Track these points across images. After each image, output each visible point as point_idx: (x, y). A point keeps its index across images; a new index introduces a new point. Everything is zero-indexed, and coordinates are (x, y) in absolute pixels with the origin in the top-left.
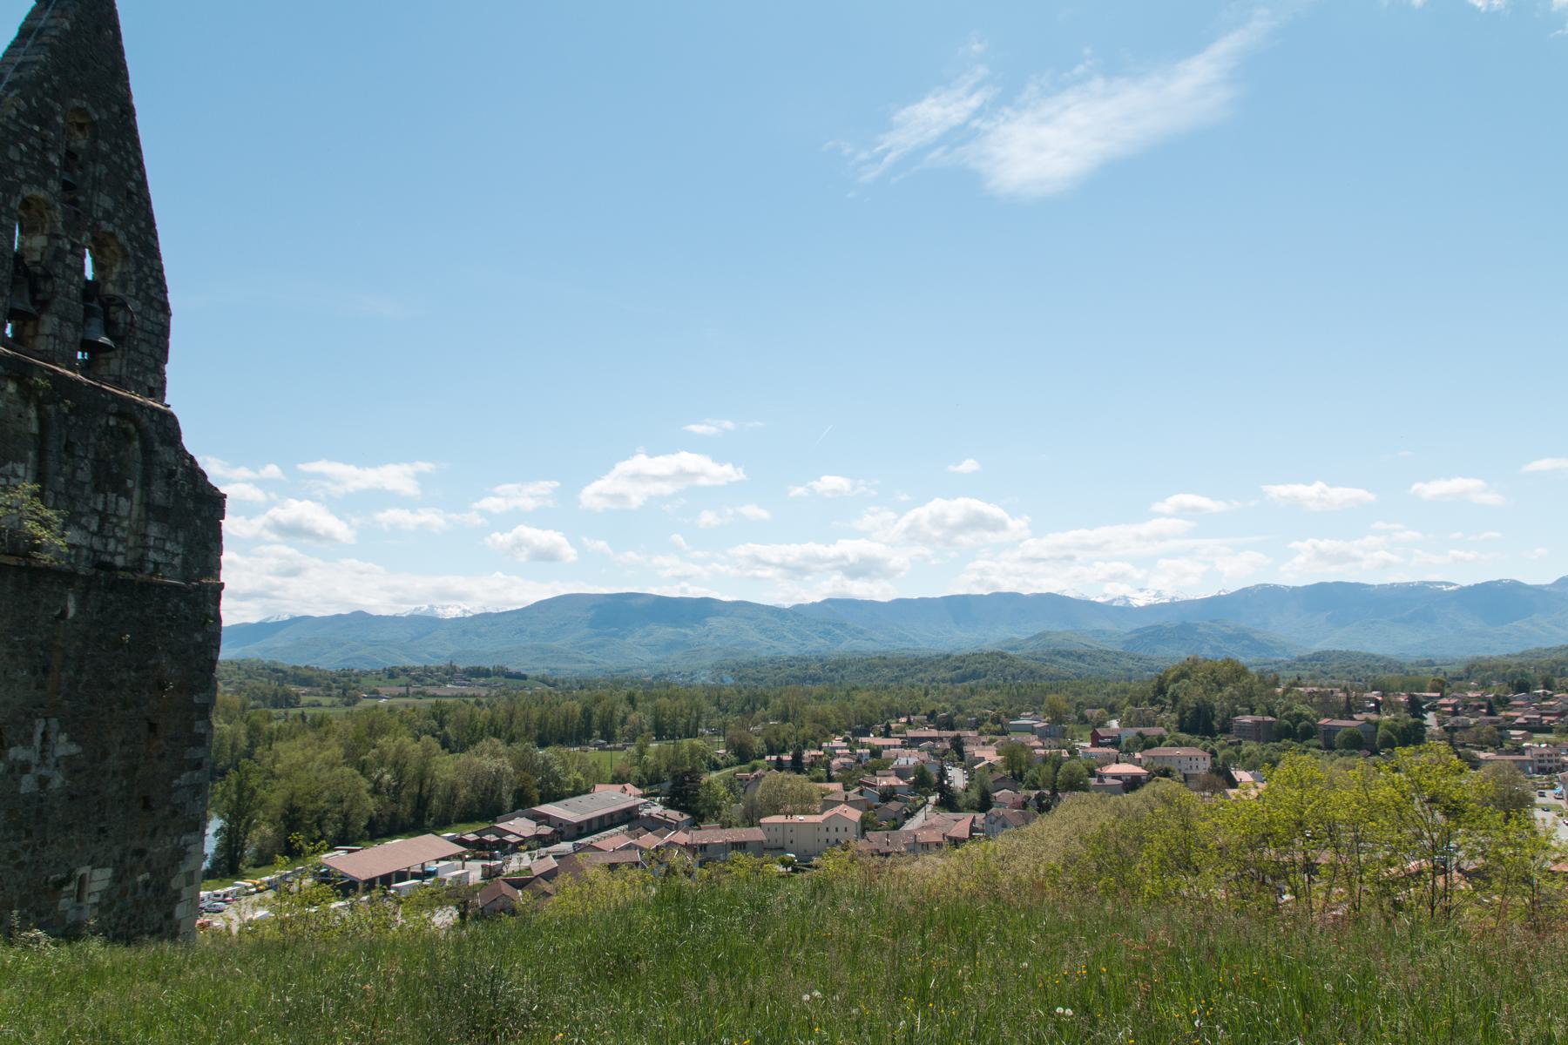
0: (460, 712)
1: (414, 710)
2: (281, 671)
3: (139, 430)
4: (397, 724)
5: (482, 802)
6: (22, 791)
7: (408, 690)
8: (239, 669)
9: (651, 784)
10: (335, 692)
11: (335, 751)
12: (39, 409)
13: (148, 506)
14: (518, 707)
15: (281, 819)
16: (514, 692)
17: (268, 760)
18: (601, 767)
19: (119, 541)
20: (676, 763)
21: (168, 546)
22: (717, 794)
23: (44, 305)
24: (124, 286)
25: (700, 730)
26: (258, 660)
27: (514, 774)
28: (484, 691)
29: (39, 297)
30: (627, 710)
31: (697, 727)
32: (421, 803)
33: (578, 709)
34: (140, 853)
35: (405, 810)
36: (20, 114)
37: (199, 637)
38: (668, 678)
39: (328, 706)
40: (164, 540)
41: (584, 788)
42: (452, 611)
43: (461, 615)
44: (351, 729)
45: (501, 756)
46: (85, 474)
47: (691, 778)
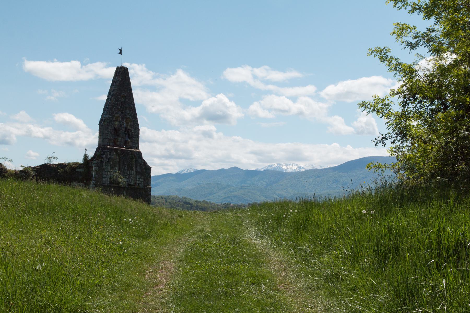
2: (189, 203)
8: (166, 201)
12: (119, 156)
13: (137, 172)
19: (132, 179)
21: (141, 180)
23: (118, 136)
26: (177, 196)
42: (292, 167)
46: (126, 168)
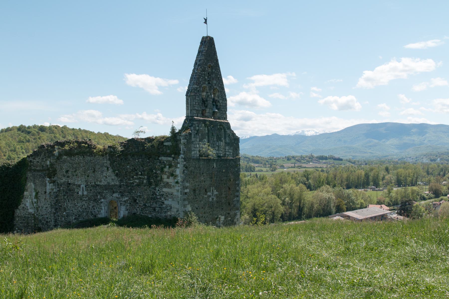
0: (315, 174)
1: (297, 174)
2: (248, 158)
3: (223, 127)
4: (291, 179)
5: (323, 210)
6: (210, 201)
7: (295, 165)
9: (394, 205)
10: (268, 166)
11: (269, 189)
13: (226, 143)
14: (338, 173)
15: (251, 212)
16: (337, 166)
17: (246, 192)
18: (372, 198)
20: (405, 197)
22: (420, 210)
24: (219, 98)
25: (418, 183)
27: (336, 199)
28: (325, 166)
29: (205, 105)
30: (385, 174)
31: (416, 181)
32: (300, 209)
33: (363, 173)
34: (229, 214)
35: (295, 211)
36: (201, 71)
37: (236, 169)
38: (405, 160)
39: (265, 172)
40: (229, 150)
41: (365, 206)
43: (315, 134)
44: (274, 181)
45: (330, 192)
46: (215, 139)
47: (409, 203)
